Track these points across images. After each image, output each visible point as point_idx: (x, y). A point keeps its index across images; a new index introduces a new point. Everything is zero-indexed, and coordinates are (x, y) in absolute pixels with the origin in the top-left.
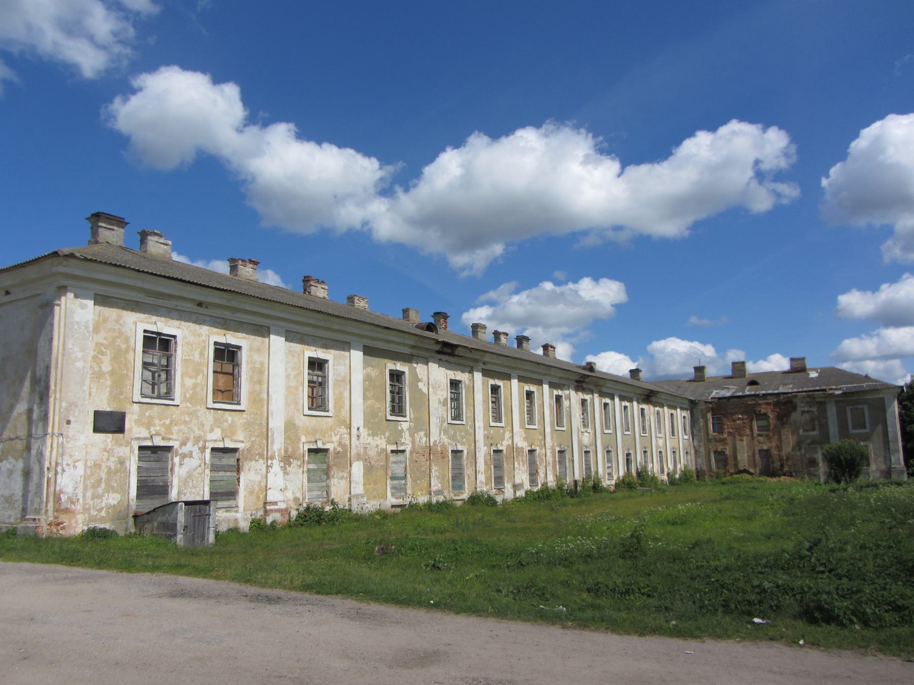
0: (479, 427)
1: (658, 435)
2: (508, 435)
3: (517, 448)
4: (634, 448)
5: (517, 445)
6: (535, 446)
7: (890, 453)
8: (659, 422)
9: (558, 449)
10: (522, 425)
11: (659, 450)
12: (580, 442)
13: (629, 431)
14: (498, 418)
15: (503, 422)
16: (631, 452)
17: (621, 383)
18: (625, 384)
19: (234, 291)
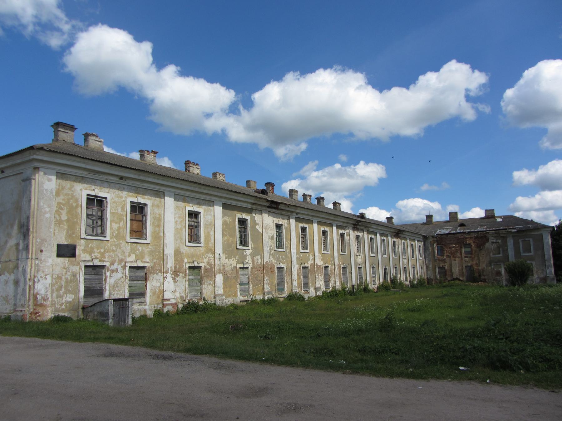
0: (294, 253)
2: (311, 257)
3: (317, 266)
9: (342, 266)
10: (320, 252)
12: (355, 261)
14: (305, 248)
16: (387, 267)
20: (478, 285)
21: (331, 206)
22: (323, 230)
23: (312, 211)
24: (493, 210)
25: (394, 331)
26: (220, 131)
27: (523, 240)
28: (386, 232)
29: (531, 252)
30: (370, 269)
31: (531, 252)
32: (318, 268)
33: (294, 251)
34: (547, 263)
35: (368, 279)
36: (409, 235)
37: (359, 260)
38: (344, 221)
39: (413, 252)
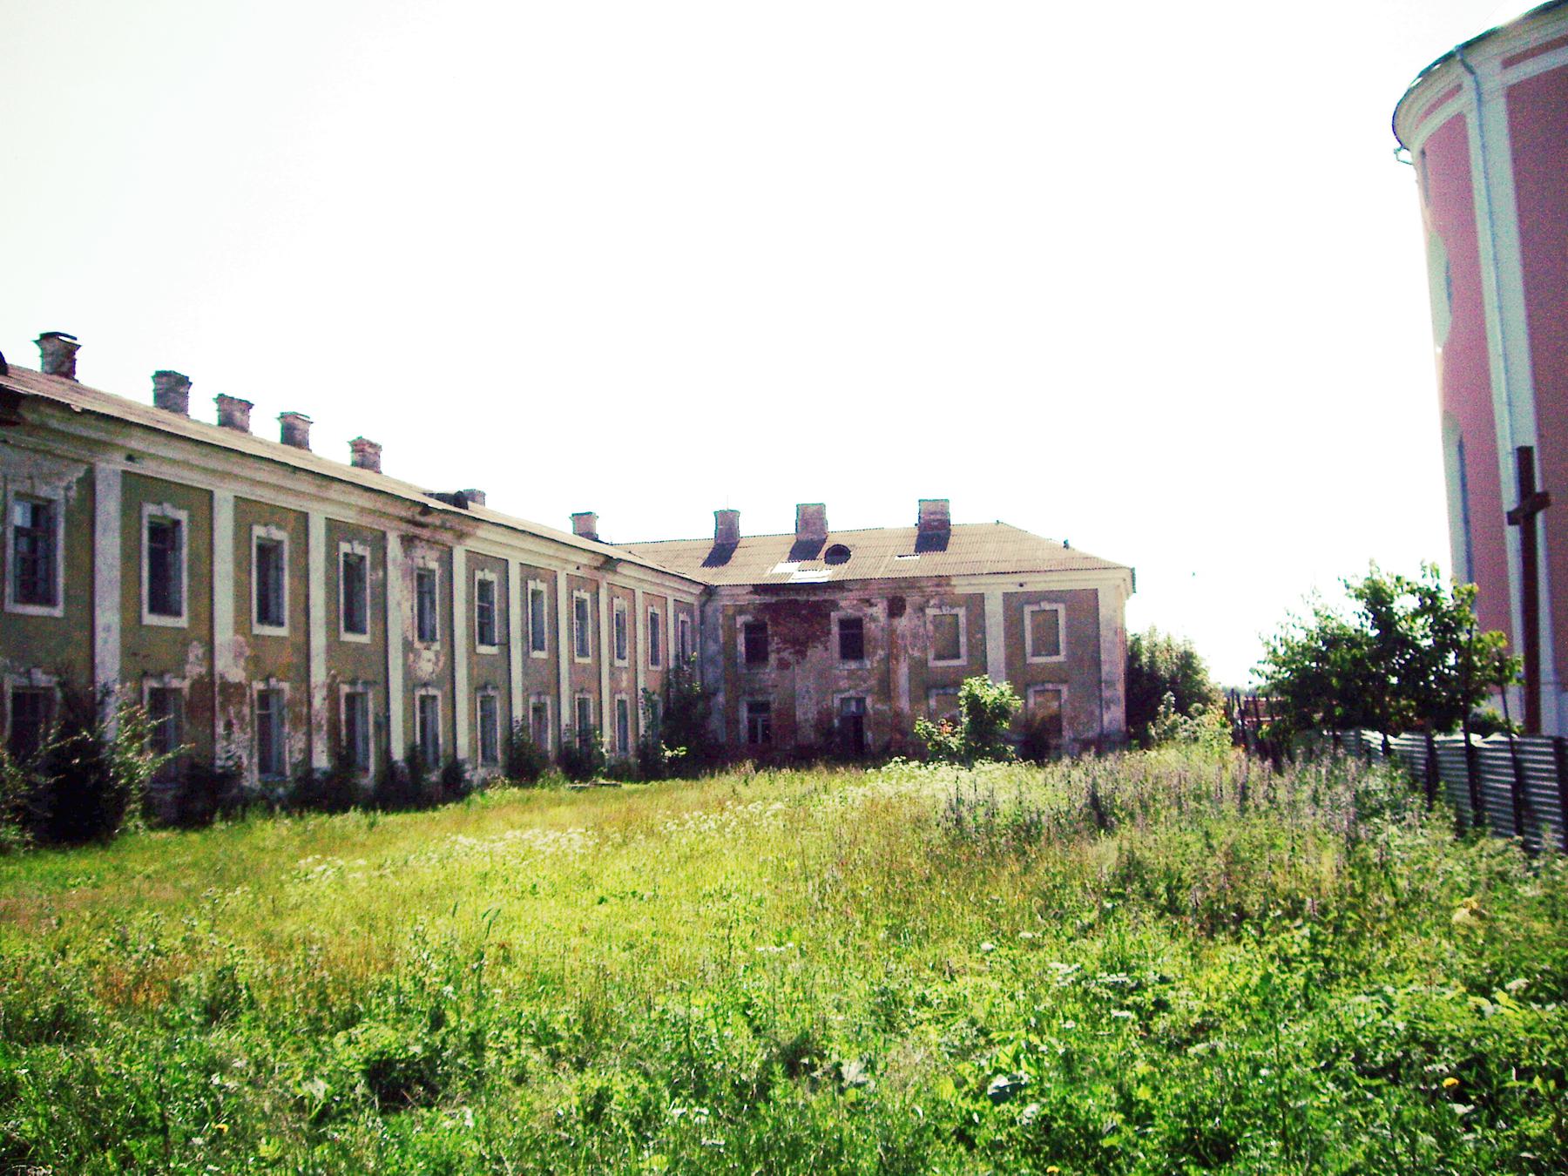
0: (108, 629)
1: (618, 663)
2: (196, 651)
3: (226, 686)
4: (554, 692)
5: (222, 677)
6: (279, 680)
7: (1101, 706)
8: (683, 636)
9: (345, 689)
10: (241, 626)
11: (618, 697)
12: (408, 672)
13: (541, 648)
14: (163, 602)
15: (1063, 653)
16: (548, 700)
17: (523, 532)
18: (534, 535)
19: (85, 412)
20: (267, 679)
21: (273, 433)
22: (150, 516)
23: (205, 450)
24: (947, 501)
25: (894, 966)
26: (1352, 617)
27: (1036, 608)
28: (548, 561)
29: (1057, 653)
30: (472, 701)
31: (1057, 653)
32: (231, 695)
33: (108, 617)
34: (1106, 694)
35: (463, 741)
36: (641, 580)
37: (427, 664)
38: (551, 552)
39: (654, 645)
